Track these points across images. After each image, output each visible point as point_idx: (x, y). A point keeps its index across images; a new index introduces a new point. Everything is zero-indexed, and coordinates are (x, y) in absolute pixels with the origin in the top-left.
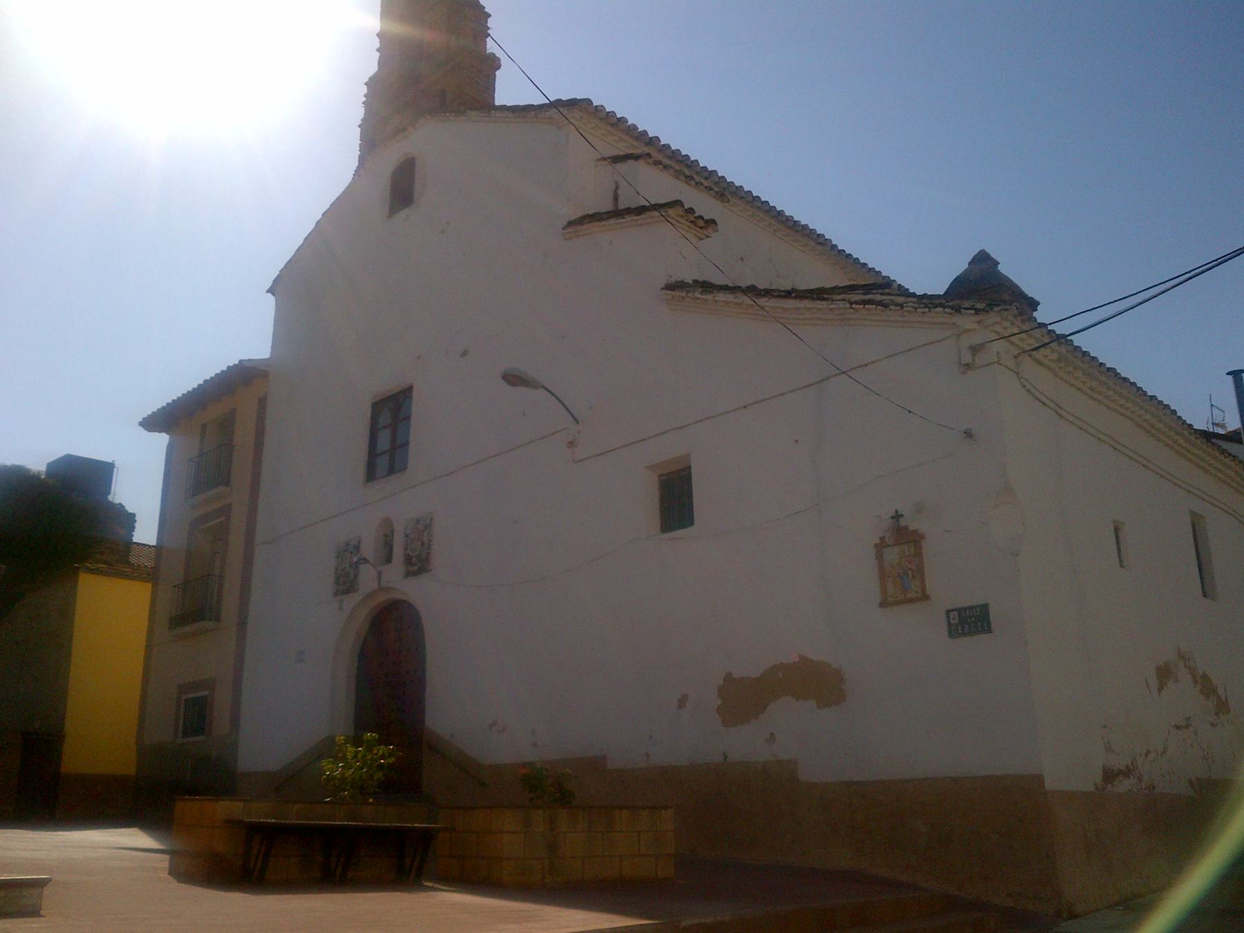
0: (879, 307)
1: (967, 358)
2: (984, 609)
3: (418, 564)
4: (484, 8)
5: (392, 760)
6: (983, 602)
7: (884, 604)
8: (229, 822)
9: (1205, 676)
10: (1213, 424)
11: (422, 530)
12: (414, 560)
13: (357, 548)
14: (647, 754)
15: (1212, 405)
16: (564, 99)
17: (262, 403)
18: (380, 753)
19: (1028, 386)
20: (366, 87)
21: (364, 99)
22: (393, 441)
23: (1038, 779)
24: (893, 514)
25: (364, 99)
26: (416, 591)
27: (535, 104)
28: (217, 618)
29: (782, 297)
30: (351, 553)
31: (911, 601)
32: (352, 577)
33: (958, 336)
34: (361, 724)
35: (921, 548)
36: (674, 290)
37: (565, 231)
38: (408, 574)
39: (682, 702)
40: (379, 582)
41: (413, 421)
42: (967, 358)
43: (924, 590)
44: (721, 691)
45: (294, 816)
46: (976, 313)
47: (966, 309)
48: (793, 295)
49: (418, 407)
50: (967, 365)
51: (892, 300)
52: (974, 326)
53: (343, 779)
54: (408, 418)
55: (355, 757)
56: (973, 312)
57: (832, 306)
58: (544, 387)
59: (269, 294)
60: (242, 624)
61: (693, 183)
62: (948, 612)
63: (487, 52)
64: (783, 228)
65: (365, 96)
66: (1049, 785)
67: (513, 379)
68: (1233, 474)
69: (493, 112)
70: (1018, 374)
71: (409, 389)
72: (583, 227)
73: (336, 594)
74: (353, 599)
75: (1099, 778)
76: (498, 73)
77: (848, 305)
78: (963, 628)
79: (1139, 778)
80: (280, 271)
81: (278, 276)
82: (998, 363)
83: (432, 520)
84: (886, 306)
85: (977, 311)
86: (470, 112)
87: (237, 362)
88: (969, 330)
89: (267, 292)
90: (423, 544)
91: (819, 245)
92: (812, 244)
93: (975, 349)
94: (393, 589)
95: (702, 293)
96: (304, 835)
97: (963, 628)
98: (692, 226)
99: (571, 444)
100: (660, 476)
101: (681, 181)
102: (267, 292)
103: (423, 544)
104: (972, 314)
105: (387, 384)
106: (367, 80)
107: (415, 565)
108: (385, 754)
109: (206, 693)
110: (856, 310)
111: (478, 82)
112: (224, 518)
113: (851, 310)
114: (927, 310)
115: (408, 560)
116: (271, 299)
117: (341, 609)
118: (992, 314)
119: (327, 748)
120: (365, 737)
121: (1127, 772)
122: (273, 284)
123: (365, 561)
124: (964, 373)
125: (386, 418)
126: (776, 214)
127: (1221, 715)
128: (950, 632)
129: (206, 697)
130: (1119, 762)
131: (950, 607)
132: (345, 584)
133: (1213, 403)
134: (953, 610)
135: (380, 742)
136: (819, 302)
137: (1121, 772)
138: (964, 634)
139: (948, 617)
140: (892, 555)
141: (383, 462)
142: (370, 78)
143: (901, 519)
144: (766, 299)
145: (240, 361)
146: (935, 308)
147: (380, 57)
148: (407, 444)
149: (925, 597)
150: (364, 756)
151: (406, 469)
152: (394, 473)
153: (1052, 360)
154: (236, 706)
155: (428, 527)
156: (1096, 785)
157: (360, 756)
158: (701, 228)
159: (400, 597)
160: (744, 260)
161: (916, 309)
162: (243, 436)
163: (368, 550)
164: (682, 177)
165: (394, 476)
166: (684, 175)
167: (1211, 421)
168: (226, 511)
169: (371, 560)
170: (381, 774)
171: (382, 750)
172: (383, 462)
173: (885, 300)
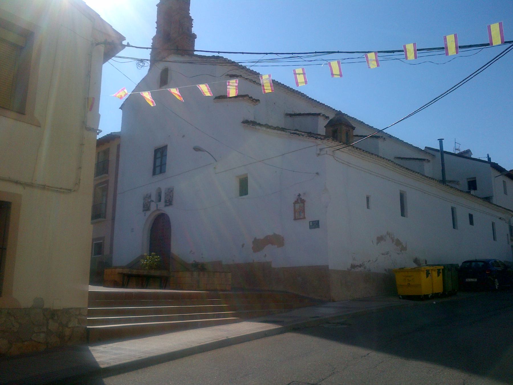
0: (298, 135)
1: (318, 152)
2: (318, 221)
3: (169, 202)
4: (191, 17)
5: (159, 260)
6: (318, 220)
7: (295, 219)
8: (119, 273)
9: (398, 240)
10: (455, 149)
11: (170, 192)
12: (168, 201)
13: (150, 196)
14: (233, 260)
15: (455, 142)
16: (215, 56)
17: (119, 146)
18: (156, 258)
19: (337, 159)
20: (152, 40)
21: (152, 44)
22: (161, 162)
23: (327, 267)
24: (298, 194)
25: (152, 44)
26: (169, 211)
27: (207, 56)
28: (105, 217)
29: (273, 129)
30: (148, 198)
31: (301, 219)
32: (148, 206)
33: (317, 146)
34: (151, 251)
35: (304, 204)
36: (244, 123)
37: (215, 100)
38: (166, 206)
39: (243, 246)
40: (157, 208)
41: (167, 165)
42: (318, 152)
43: (304, 216)
44: (253, 242)
45: (135, 272)
46: (321, 140)
47: (319, 138)
48: (277, 129)
49: (170, 153)
50: (318, 154)
51: (301, 133)
52: (320, 143)
53: (146, 264)
54: (166, 155)
55: (149, 259)
56: (320, 139)
57: (286, 134)
58: (206, 151)
59: (120, 109)
60: (113, 219)
61: (255, 83)
62: (310, 222)
63: (192, 33)
64: (290, 92)
65: (152, 43)
66: (330, 268)
67: (197, 149)
68: (419, 178)
69: (193, 57)
70: (333, 156)
71: (165, 147)
72: (219, 100)
73: (144, 211)
74: (148, 213)
75: (349, 267)
76: (195, 40)
77: (290, 134)
78: (313, 227)
79: (364, 268)
80: (124, 102)
81: (123, 104)
82: (326, 154)
83: (173, 189)
84: (299, 135)
85: (321, 139)
86: (186, 55)
87: (110, 133)
88: (320, 144)
89: (120, 108)
90: (170, 197)
91: (303, 97)
92: (300, 96)
93: (321, 150)
94: (161, 210)
95: (252, 125)
96: (138, 276)
97: (313, 227)
98: (252, 102)
99: (215, 168)
100: (240, 179)
101: (252, 83)
102: (120, 108)
103: (170, 197)
104: (320, 140)
105: (159, 144)
106: (152, 38)
107: (168, 203)
108: (157, 258)
109: (102, 241)
110: (292, 135)
111: (189, 44)
112: (106, 184)
113: (291, 135)
114: (309, 137)
115: (166, 202)
116: (121, 111)
117: (145, 216)
118: (325, 140)
119: (142, 257)
120: (152, 254)
121: (360, 266)
122: (121, 106)
123: (153, 201)
124: (318, 156)
125: (159, 155)
126: (286, 88)
127: (402, 251)
128: (310, 227)
129: (102, 243)
130: (357, 263)
131: (310, 221)
132: (146, 208)
133: (456, 142)
134: (311, 222)
135: (156, 255)
136: (283, 132)
137: (357, 266)
138: (313, 228)
139: (310, 223)
140: (297, 206)
141: (158, 169)
142: (154, 37)
143: (300, 196)
144: (269, 129)
145: (111, 133)
146: (311, 137)
147: (157, 30)
148: (165, 164)
149: (304, 218)
150: (152, 258)
151: (165, 172)
152: (162, 173)
153: (347, 151)
154: (112, 245)
155: (172, 191)
156: (348, 269)
157: (151, 258)
158: (255, 102)
159: (164, 212)
160: (276, 104)
161: (306, 137)
162: (112, 157)
163: (154, 198)
164: (252, 82)
165: (162, 174)
166: (253, 81)
167: (455, 148)
168: (107, 182)
169: (154, 201)
170: (156, 263)
171: (156, 257)
172: (158, 169)
173: (299, 133)
